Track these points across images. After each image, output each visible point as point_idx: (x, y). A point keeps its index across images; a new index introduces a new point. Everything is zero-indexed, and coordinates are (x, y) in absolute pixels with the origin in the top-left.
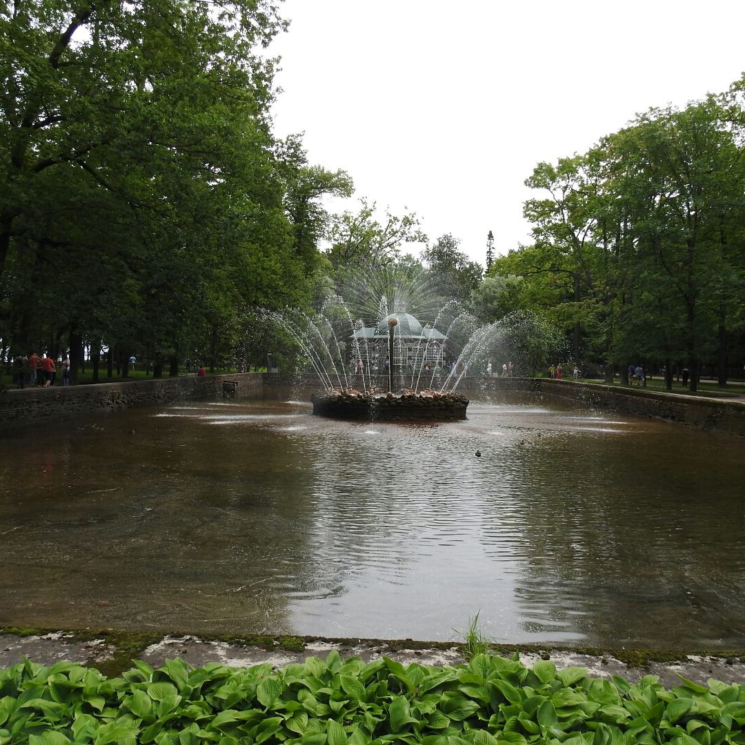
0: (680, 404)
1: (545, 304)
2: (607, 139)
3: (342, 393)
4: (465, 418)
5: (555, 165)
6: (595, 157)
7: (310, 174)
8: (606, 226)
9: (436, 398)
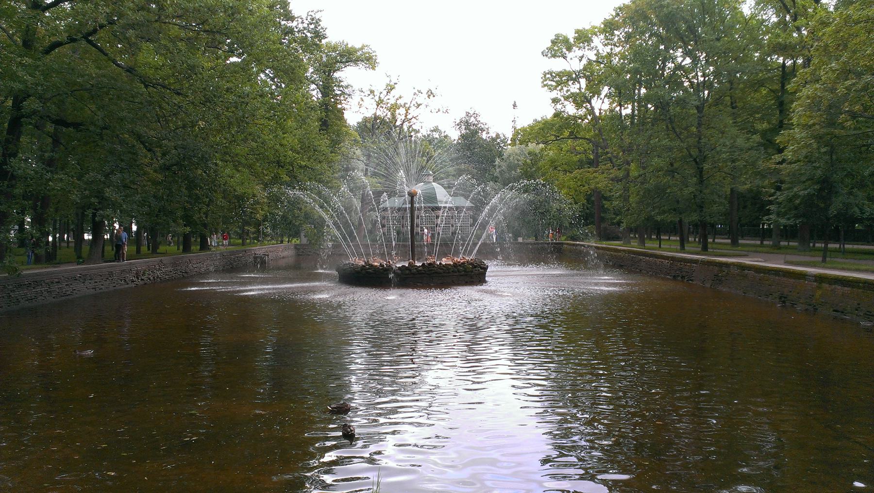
0: (689, 264)
1: (565, 171)
2: (620, 9)
3: (365, 263)
4: (486, 282)
5: (571, 36)
6: (609, 27)
7: (334, 49)
8: (622, 94)
9: (455, 265)
